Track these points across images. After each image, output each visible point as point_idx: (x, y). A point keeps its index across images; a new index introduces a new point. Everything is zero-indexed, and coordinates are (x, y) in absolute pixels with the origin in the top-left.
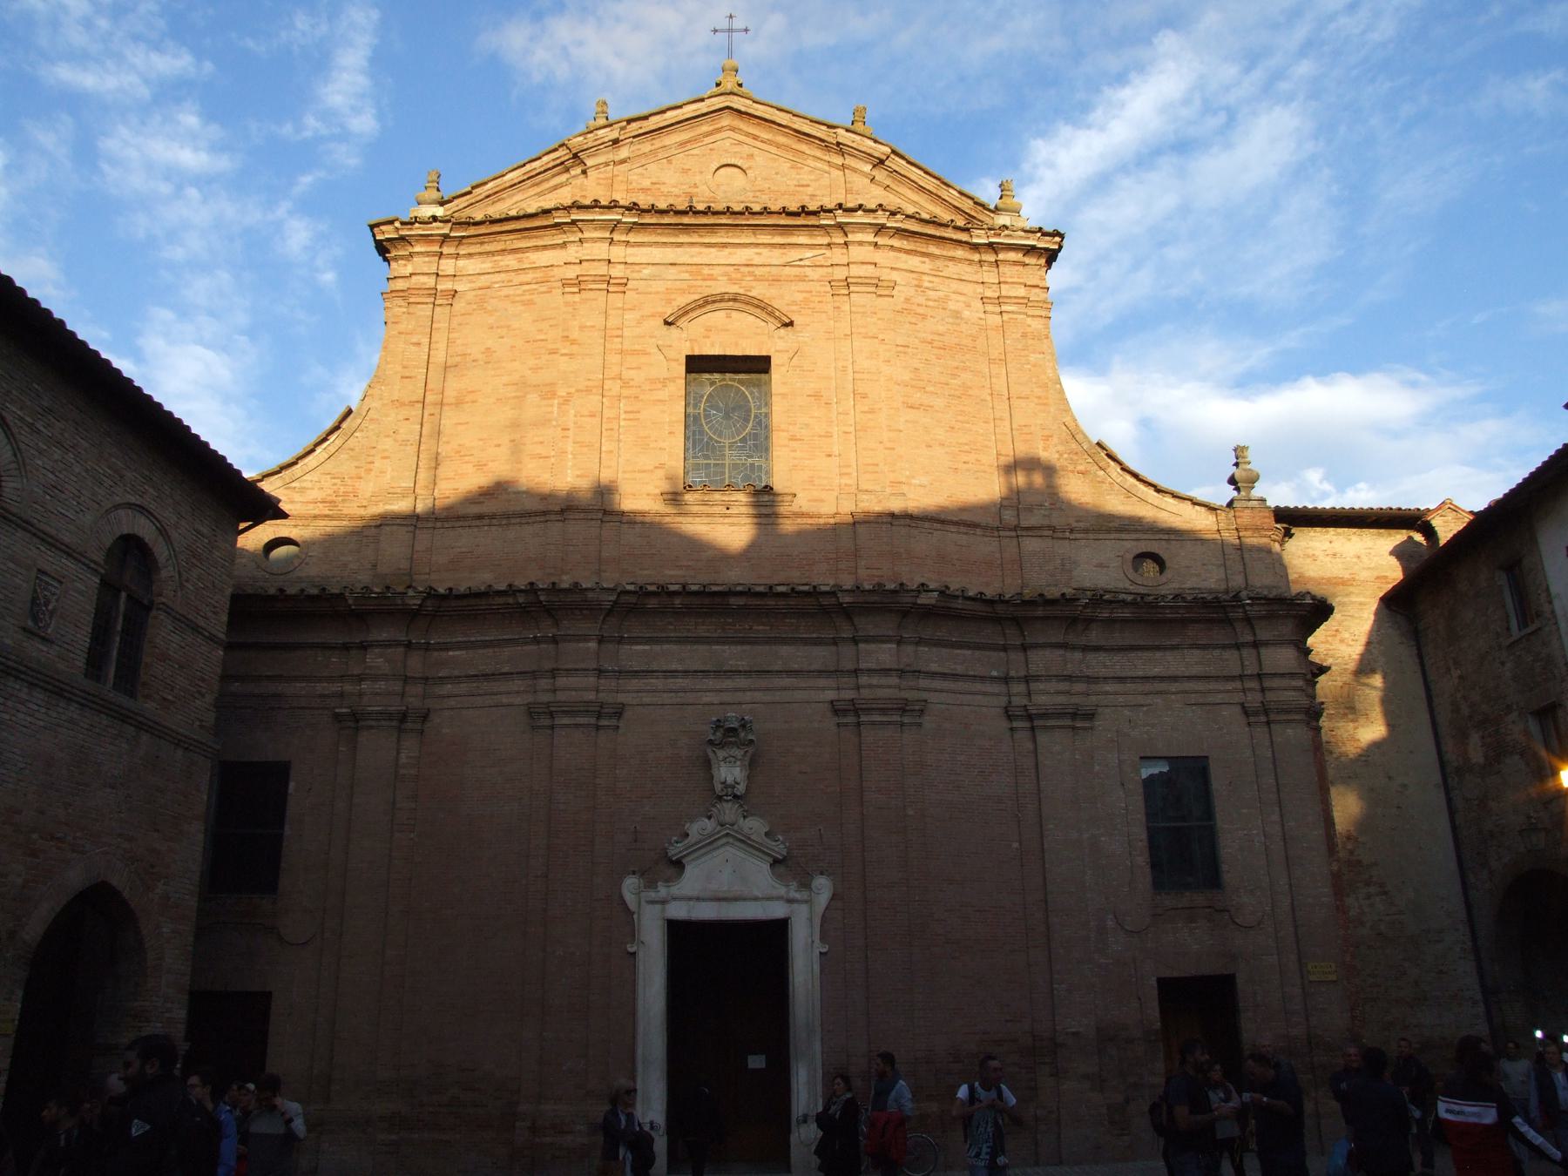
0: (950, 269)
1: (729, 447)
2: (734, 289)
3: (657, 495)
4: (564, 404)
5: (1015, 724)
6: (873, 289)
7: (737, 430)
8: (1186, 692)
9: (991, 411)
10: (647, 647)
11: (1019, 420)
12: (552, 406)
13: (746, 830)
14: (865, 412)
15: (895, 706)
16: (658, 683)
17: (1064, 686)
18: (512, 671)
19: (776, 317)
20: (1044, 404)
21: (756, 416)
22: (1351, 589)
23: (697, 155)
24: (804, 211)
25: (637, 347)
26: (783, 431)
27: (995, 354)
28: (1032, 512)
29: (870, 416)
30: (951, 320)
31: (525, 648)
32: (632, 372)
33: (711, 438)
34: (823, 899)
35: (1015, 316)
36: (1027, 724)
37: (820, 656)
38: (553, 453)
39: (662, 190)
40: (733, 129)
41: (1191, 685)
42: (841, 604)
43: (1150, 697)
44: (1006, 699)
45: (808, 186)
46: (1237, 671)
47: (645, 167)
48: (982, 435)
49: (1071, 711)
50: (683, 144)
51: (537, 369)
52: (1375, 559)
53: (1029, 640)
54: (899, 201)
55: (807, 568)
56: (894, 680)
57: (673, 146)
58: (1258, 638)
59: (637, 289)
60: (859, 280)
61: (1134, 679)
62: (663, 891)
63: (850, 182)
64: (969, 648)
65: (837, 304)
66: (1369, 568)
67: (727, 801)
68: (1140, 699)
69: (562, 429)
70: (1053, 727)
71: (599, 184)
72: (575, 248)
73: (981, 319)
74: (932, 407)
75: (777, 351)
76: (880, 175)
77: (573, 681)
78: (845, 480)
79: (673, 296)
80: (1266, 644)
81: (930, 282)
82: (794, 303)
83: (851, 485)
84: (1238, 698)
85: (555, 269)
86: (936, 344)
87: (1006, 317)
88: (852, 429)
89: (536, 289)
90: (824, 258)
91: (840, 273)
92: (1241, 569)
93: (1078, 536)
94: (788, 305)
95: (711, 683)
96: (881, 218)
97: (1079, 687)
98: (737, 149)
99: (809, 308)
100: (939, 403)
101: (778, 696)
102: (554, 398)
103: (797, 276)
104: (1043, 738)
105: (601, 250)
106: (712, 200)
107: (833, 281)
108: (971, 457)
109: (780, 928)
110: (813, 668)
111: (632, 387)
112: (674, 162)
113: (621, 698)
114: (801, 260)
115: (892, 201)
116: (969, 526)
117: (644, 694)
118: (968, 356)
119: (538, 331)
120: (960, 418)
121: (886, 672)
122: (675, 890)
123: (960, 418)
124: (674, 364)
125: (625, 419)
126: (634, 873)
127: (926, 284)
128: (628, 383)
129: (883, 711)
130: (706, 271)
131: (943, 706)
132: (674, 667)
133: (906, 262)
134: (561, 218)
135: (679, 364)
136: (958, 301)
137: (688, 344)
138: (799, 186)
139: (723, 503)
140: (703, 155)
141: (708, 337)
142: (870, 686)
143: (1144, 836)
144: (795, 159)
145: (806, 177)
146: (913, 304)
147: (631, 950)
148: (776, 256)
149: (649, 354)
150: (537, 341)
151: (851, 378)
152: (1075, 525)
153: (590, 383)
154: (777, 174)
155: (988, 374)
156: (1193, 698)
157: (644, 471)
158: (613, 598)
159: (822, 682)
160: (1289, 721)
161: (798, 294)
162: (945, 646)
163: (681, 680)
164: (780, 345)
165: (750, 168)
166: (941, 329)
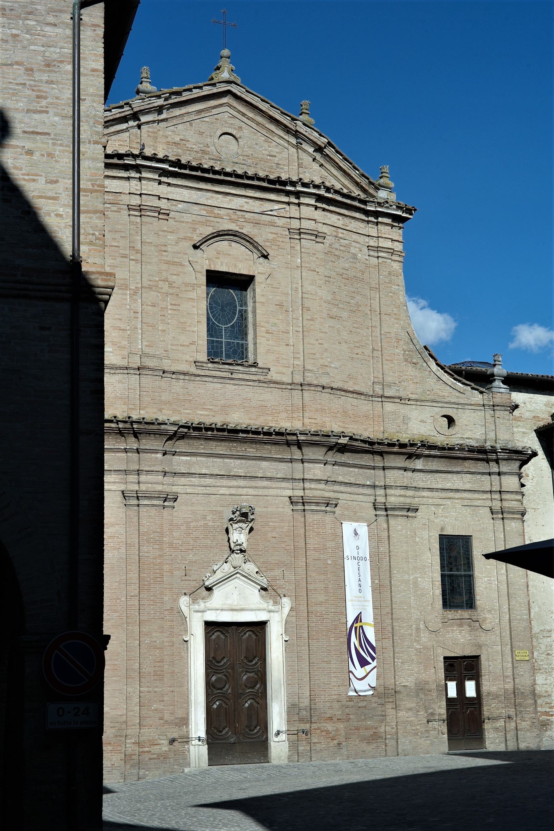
0: (352, 225)
1: (225, 330)
2: (233, 227)
3: (191, 362)
4: (134, 295)
5: (378, 513)
6: (314, 238)
7: (229, 319)
8: (462, 499)
9: (370, 321)
10: (188, 458)
11: (385, 329)
12: (126, 294)
13: (246, 570)
14: (309, 320)
15: (324, 502)
16: (195, 480)
17: (403, 492)
18: (111, 469)
19: (258, 250)
20: (398, 319)
21: (240, 311)
22: (519, 423)
23: (208, 122)
24: (279, 181)
25: (176, 260)
26: (263, 327)
27: (373, 285)
28: (390, 387)
29: (312, 323)
30: (352, 260)
31: (117, 454)
32: (174, 277)
33: (213, 323)
34: (286, 610)
35: (385, 260)
36: (384, 513)
37: (283, 469)
38: (128, 328)
39: (187, 146)
40: (230, 106)
41: (465, 494)
42: (298, 440)
43: (445, 500)
44: (373, 497)
45: (275, 156)
46: (488, 489)
47: (176, 126)
48: (365, 337)
49: (407, 507)
50: (200, 112)
51: (114, 266)
52: (534, 405)
53: (386, 464)
54: (327, 174)
55: (275, 415)
56: (322, 486)
57: (193, 113)
58: (501, 470)
59: (175, 218)
60: (307, 231)
61: (437, 489)
62: (202, 605)
63: (301, 159)
64: (357, 467)
65: (292, 245)
66: (530, 411)
67: (237, 553)
68: (440, 502)
69: (134, 312)
70: (398, 516)
71: (149, 136)
72: (135, 182)
73: (367, 260)
74: (341, 317)
75: (259, 273)
76: (318, 156)
77: (150, 478)
78: (296, 362)
79: (197, 226)
80: (505, 474)
81: (342, 233)
82: (267, 240)
83: (299, 365)
84: (489, 503)
85: (123, 195)
86: (344, 276)
87: (381, 260)
88: (301, 329)
89: (109, 208)
90: (285, 211)
91: (295, 224)
92: (494, 429)
93: (412, 403)
94: (264, 241)
95: (225, 482)
96: (322, 192)
97: (410, 493)
98: (232, 121)
99: (276, 245)
100: (345, 315)
101: (260, 492)
102: (127, 290)
103: (270, 222)
104: (392, 521)
105: (151, 187)
106: (218, 158)
107: (291, 229)
108: (359, 351)
109: (262, 625)
110: (278, 476)
111: (174, 287)
112: (193, 125)
113: (175, 489)
114: (271, 211)
115: (330, 182)
116: (358, 394)
117: (188, 487)
118: (360, 285)
119: (113, 239)
120: (355, 325)
121: (318, 481)
122: (208, 605)
123: (355, 325)
124: (199, 275)
125: (171, 309)
126: (185, 594)
127: (340, 235)
128: (172, 284)
129: (317, 504)
130: (216, 211)
131: (344, 501)
132: (203, 472)
133: (330, 219)
134: (129, 161)
135: (202, 275)
136: (356, 247)
137: (207, 262)
138: (270, 156)
139: (230, 371)
140: (212, 123)
141: (219, 258)
142: (310, 489)
143: (440, 579)
144: (267, 135)
145: (275, 150)
146: (333, 248)
147: (186, 639)
148: (256, 206)
149: (184, 265)
150: (113, 246)
151: (300, 296)
152: (410, 396)
153: (151, 283)
154: (257, 144)
155: (369, 296)
156: (466, 502)
157: (183, 346)
158: (176, 429)
159: (284, 485)
160: (514, 518)
161: (270, 235)
162: (346, 466)
163: (208, 480)
164: (261, 269)
165: (240, 137)
166: (347, 266)
